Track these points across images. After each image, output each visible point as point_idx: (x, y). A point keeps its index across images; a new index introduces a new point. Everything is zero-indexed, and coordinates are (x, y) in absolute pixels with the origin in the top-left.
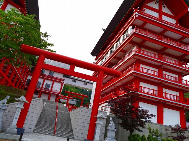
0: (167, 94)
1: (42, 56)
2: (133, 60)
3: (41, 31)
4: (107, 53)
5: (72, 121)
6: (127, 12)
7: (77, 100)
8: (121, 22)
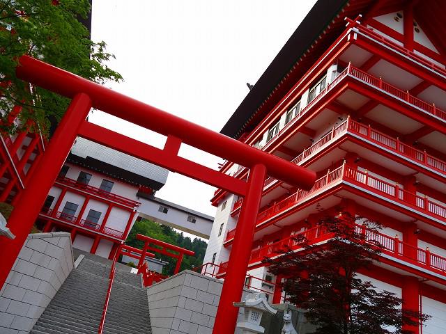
0: (433, 255)
1: (83, 98)
2: (337, 153)
3: (92, 39)
4: (260, 138)
5: (153, 314)
6: (308, 51)
7: (165, 263)
8: (303, 57)
